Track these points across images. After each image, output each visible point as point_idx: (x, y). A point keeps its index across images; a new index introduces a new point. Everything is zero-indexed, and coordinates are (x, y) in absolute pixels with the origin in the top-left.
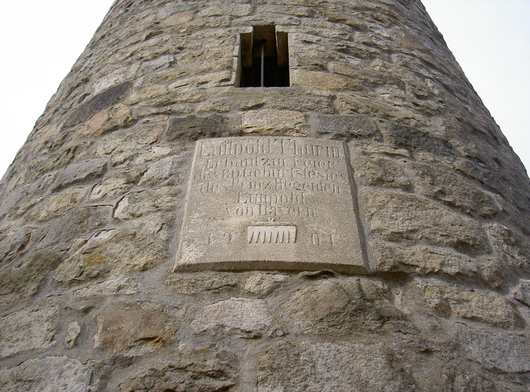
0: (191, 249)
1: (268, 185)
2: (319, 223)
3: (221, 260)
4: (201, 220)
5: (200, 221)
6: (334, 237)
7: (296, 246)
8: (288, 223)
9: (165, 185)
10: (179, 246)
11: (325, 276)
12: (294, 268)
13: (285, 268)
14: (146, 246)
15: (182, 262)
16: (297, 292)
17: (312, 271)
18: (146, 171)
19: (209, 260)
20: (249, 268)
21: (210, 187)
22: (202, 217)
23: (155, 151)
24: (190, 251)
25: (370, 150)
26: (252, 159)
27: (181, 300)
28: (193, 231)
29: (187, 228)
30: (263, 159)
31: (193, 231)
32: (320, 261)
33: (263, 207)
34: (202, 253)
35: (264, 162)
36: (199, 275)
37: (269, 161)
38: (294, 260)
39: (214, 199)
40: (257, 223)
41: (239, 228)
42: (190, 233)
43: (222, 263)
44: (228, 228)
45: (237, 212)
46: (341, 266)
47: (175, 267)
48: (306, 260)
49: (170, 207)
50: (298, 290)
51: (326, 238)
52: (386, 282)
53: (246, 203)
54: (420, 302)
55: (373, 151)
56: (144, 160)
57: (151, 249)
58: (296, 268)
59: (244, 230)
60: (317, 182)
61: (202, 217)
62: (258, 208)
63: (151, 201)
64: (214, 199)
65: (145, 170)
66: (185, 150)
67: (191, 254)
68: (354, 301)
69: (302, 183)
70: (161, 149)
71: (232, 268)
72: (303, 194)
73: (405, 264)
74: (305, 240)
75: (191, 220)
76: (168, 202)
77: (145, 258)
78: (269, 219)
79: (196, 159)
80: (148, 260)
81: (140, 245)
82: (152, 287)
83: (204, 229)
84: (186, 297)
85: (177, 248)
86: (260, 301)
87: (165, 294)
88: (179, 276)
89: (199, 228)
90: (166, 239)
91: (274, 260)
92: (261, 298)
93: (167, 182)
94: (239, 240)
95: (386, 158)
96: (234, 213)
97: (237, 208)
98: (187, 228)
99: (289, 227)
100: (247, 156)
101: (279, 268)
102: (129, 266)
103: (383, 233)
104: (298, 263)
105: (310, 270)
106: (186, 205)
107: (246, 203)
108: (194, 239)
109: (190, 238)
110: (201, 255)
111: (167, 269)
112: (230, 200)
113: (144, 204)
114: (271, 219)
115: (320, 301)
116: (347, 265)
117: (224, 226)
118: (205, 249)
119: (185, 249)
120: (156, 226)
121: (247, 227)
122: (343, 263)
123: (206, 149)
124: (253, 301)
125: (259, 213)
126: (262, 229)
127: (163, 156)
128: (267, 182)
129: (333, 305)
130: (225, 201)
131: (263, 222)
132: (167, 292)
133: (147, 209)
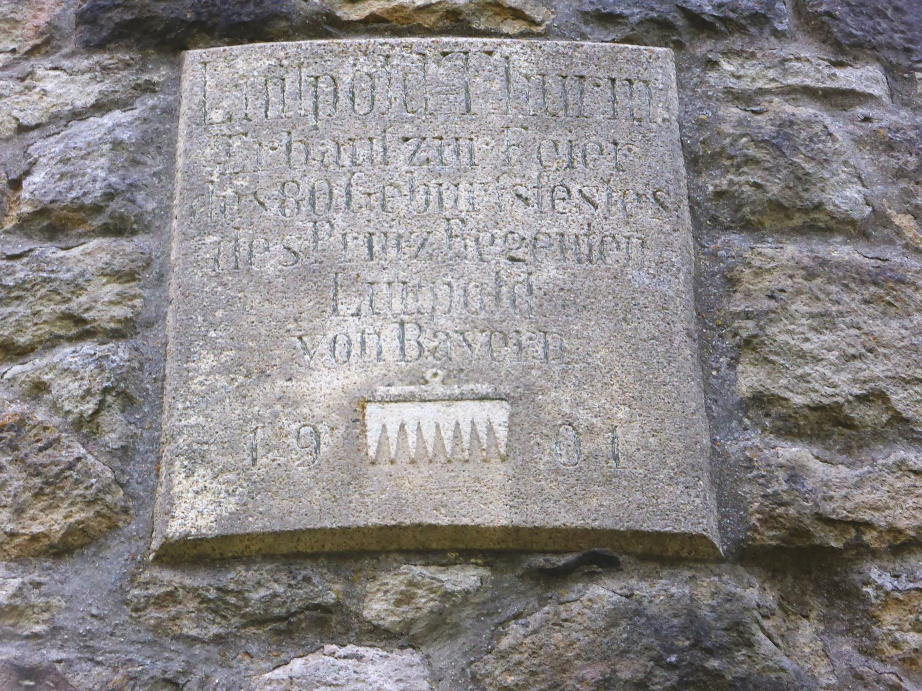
0: (201, 485)
1: (423, 245)
2: (579, 386)
3: (294, 523)
4: (222, 381)
5: (219, 385)
6: (624, 434)
7: (511, 472)
8: (484, 388)
9: (129, 306)
10: (163, 469)
11: (595, 568)
12: (504, 546)
13: (477, 545)
14: (62, 471)
15: (175, 529)
16: (513, 624)
17: (556, 553)
18: (27, 173)
19: (256, 525)
20: (374, 547)
21: (243, 252)
22: (225, 370)
23: (49, 86)
24: (197, 493)
25: (754, 80)
26: (370, 139)
27: (183, 658)
28: (201, 420)
29: (180, 406)
30: (406, 140)
31: (201, 420)
32: (579, 523)
33: (411, 332)
34: (233, 500)
35: (411, 146)
36: (230, 578)
37: (423, 145)
38: (504, 522)
39: (258, 298)
40: (394, 391)
41: (340, 409)
42: (192, 427)
43: (296, 535)
44: (306, 411)
45: (333, 350)
46: (638, 535)
47: (155, 545)
48: (539, 520)
49: (119, 321)
50: (517, 617)
51: (600, 440)
52: (773, 577)
53: (357, 314)
54: (868, 643)
55: (760, 84)
56: (14, 125)
57: (77, 482)
58: (511, 545)
59: (355, 416)
60: (574, 230)
61: (225, 370)
62: (396, 333)
63: (58, 298)
64: (258, 298)
65: (24, 166)
66: (149, 88)
67: (202, 502)
68: (673, 659)
69: (528, 235)
70: (66, 82)
71: (327, 549)
72: (533, 278)
73: (833, 520)
74: (536, 448)
75: (192, 379)
76: (111, 303)
77: (63, 511)
78: (428, 376)
79: (190, 135)
80: (72, 520)
81: (44, 465)
82: (94, 611)
83: (233, 412)
84: (197, 649)
85: (158, 476)
86: (409, 656)
87: (134, 637)
88: (170, 578)
89: (218, 408)
90: (120, 444)
91: (444, 521)
92: (413, 644)
93: (98, 221)
94: (342, 453)
95: (806, 110)
96: (322, 355)
97: (330, 336)
98: (180, 406)
99: (487, 404)
100: (354, 128)
101: (461, 546)
102: (17, 541)
103: (773, 411)
104: (517, 530)
105: (550, 548)
106: (170, 317)
107: (357, 314)
108: (206, 447)
109: (195, 447)
110: (232, 507)
111: (133, 550)
112: (308, 303)
113: (38, 308)
114: (435, 375)
115: (578, 657)
116: (659, 534)
117: (296, 404)
118: (241, 486)
119: (181, 484)
120: (83, 398)
121: (364, 408)
122: (646, 527)
123: (218, 93)
124: (387, 657)
125: (398, 352)
126: (410, 412)
127: (78, 115)
128: (418, 234)
129: (614, 671)
130: (292, 310)
131: (412, 388)
132: (139, 631)
133: (47, 328)
